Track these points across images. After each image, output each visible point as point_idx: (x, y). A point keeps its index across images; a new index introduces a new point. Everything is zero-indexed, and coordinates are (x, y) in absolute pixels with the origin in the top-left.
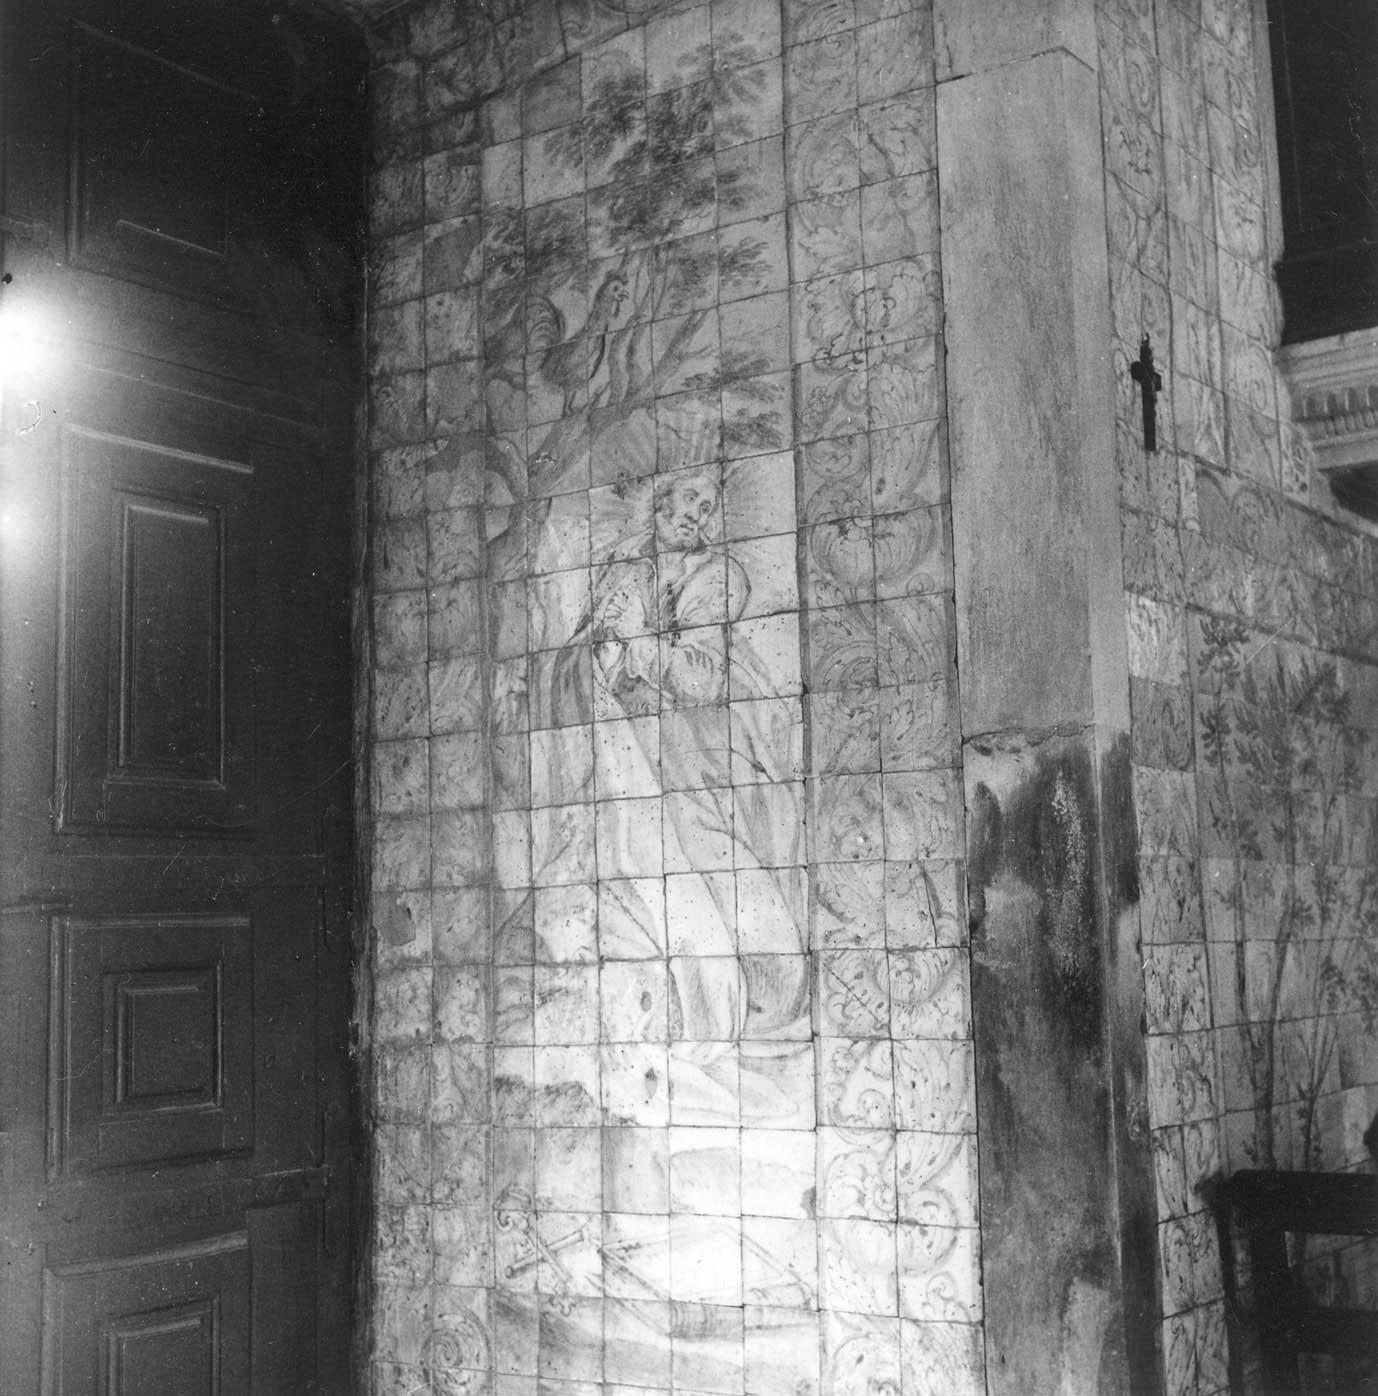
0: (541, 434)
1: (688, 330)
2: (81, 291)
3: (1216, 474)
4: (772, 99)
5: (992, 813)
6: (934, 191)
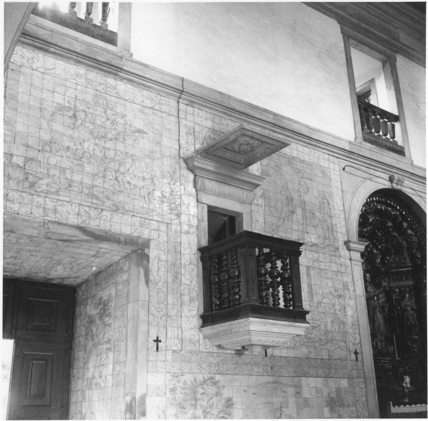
0: (90, 348)
1: (105, 334)
2: (59, 14)
3: (179, 352)
4: (114, 303)
5: (127, 404)
6: (127, 319)
